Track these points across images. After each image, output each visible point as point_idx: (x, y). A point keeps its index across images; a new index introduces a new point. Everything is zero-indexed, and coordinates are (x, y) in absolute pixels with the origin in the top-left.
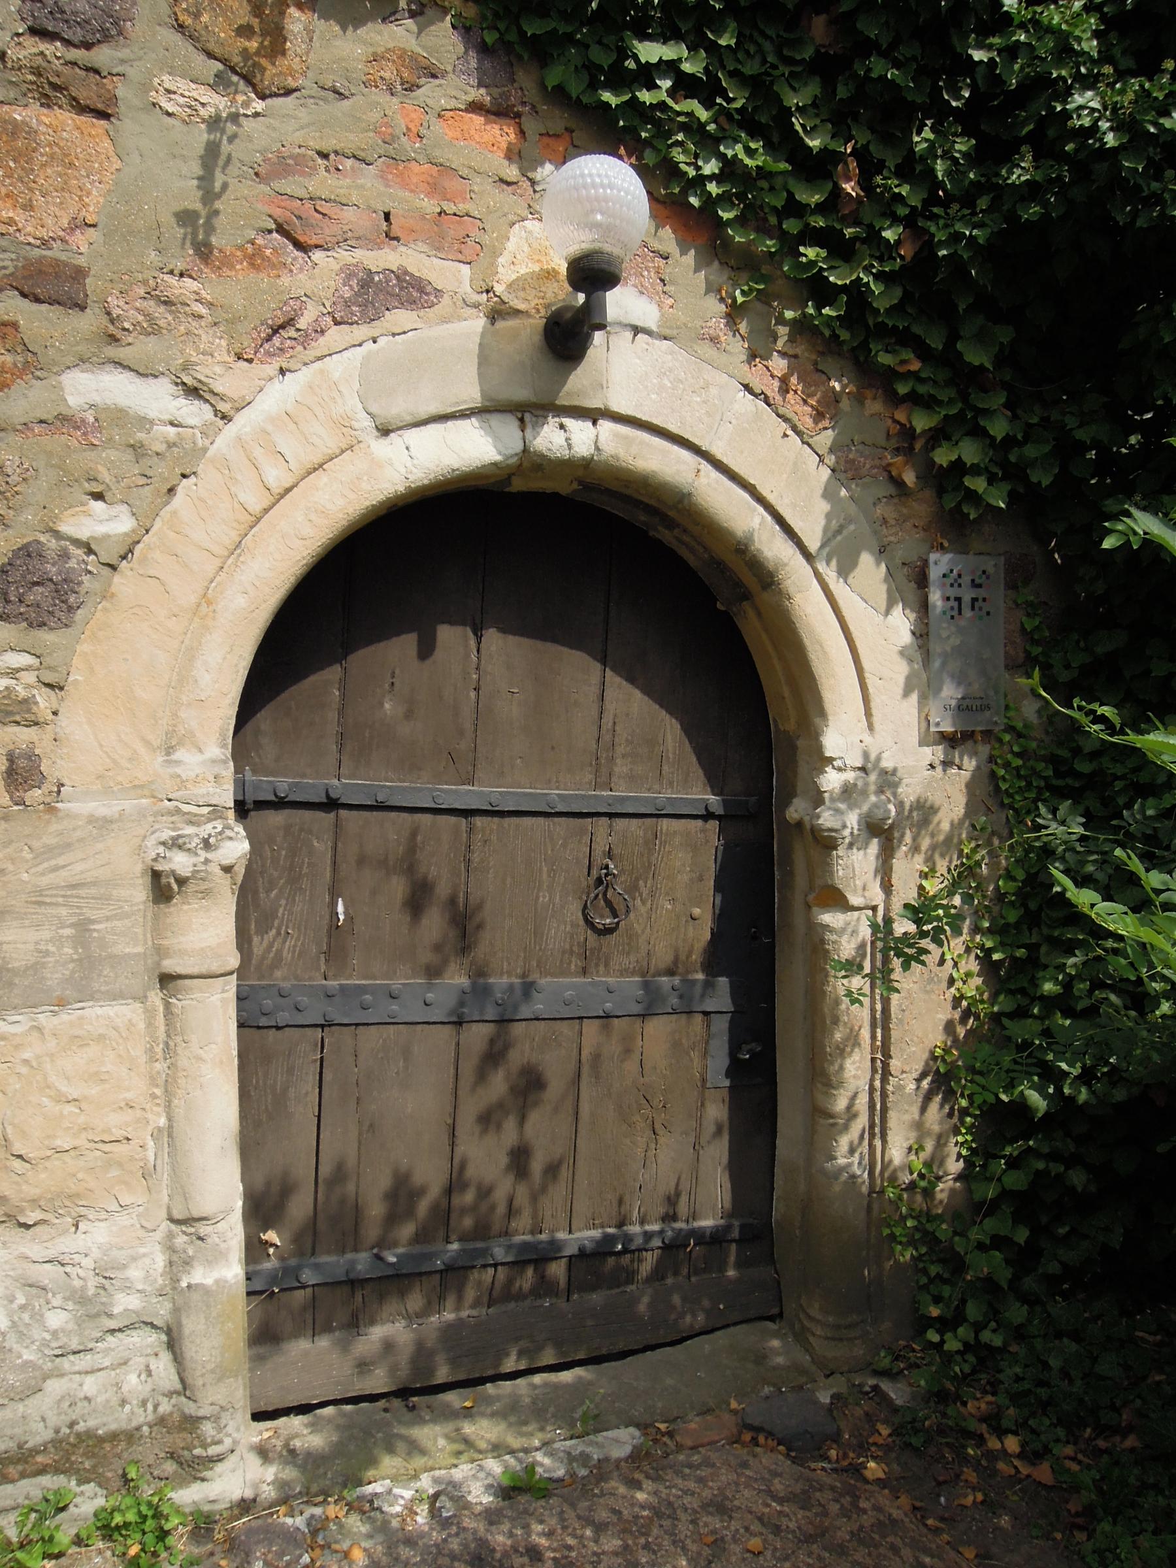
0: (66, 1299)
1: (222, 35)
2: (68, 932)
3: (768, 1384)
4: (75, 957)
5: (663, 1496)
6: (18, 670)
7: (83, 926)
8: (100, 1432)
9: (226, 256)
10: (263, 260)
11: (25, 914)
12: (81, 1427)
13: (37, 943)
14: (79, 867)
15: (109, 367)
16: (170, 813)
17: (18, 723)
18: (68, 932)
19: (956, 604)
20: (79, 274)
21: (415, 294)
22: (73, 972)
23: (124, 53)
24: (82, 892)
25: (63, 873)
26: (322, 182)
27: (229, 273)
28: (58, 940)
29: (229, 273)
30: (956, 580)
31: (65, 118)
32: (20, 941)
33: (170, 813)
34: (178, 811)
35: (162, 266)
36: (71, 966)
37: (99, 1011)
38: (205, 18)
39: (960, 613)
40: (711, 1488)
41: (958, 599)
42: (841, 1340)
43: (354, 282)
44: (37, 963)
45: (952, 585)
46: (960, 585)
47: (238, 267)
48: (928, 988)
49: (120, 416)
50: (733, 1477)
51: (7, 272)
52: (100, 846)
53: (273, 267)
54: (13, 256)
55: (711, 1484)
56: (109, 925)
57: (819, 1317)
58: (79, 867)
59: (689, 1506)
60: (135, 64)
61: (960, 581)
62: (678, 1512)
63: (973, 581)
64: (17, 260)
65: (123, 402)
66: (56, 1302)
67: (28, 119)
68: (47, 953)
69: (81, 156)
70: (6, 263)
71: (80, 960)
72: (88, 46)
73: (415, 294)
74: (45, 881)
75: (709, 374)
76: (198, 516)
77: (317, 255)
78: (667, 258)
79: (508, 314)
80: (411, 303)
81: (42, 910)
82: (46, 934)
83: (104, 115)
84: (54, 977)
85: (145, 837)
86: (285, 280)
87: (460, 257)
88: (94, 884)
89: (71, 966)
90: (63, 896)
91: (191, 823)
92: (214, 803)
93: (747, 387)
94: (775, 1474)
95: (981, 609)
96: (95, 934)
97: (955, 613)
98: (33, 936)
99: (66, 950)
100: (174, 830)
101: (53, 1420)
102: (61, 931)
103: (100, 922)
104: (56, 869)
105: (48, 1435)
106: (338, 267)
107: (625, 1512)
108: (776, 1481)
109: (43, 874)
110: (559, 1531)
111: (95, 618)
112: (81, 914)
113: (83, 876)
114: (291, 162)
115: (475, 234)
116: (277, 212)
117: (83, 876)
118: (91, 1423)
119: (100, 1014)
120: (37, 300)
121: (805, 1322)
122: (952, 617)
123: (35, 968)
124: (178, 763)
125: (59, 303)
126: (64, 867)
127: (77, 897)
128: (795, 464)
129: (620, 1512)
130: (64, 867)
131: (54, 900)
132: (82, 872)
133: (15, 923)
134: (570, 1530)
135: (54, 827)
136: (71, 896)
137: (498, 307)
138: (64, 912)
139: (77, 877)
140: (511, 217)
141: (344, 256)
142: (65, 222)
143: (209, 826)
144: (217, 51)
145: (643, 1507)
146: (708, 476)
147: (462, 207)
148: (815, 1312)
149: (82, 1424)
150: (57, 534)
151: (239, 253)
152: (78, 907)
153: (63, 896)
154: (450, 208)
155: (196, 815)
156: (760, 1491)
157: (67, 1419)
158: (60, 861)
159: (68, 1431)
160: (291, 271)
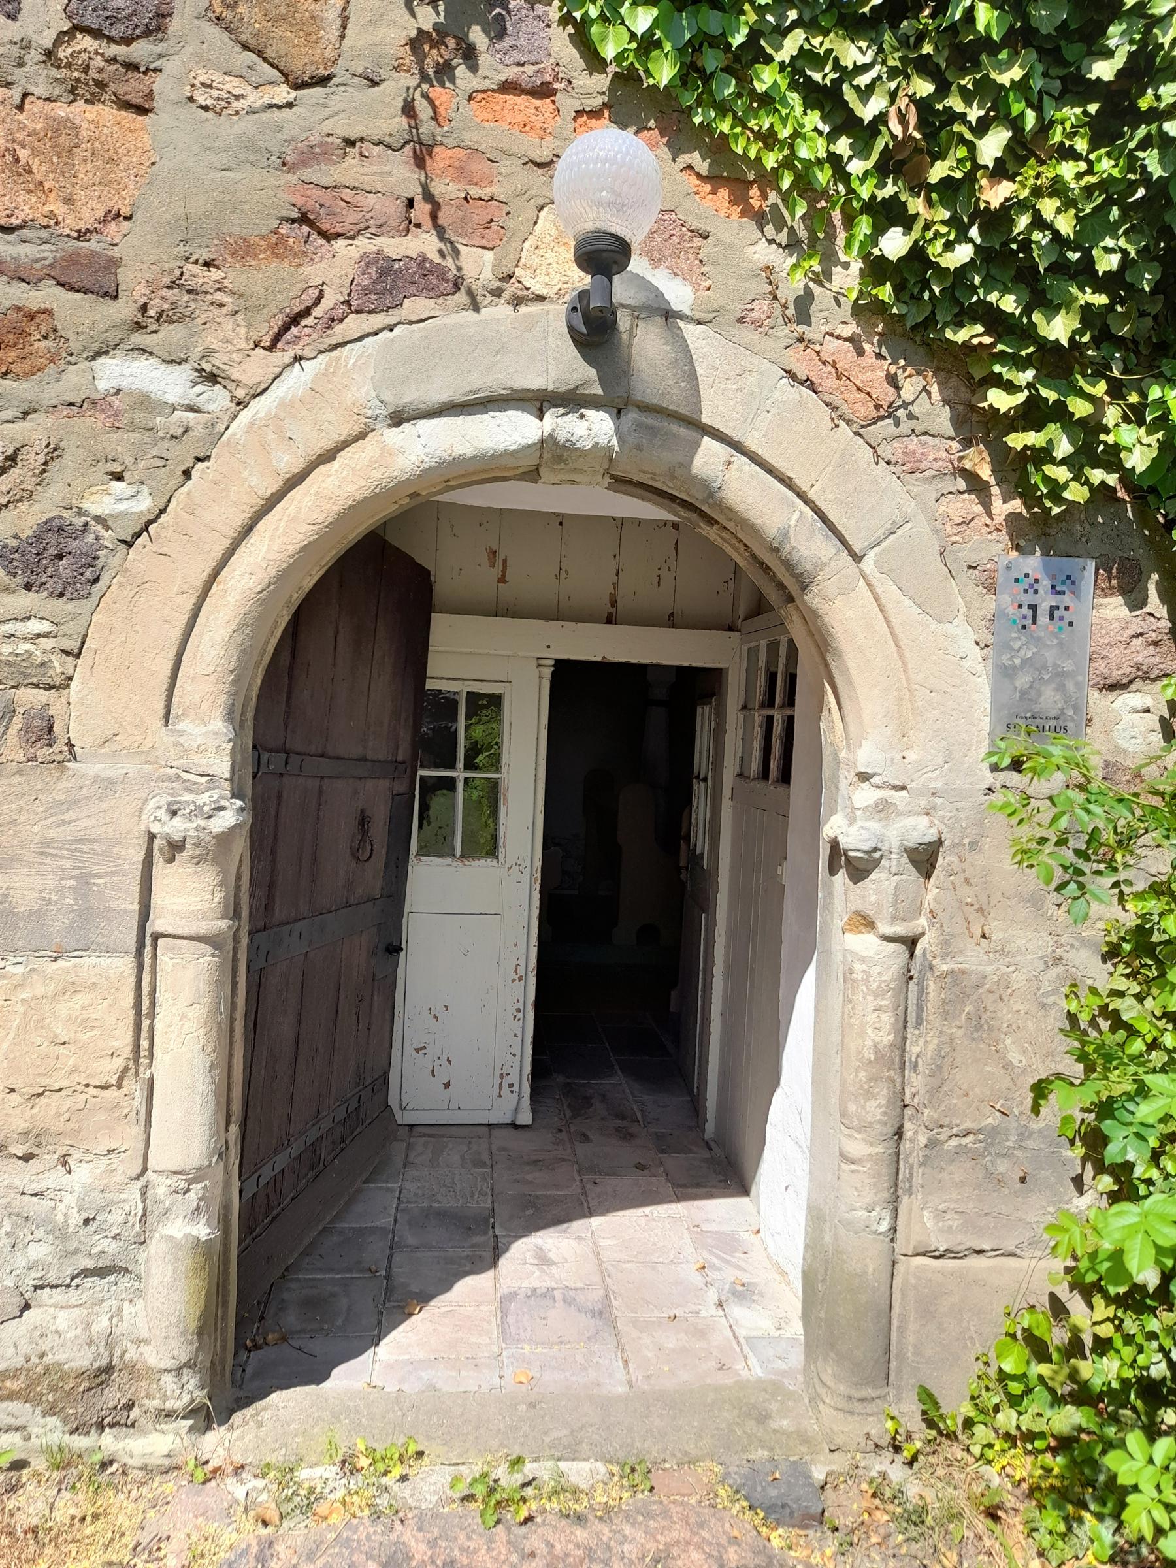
0: (47, 1233)
1: (257, 26)
2: (70, 883)
3: (763, 1447)
4: (76, 907)
5: (605, 1539)
6: (39, 636)
7: (84, 879)
8: (66, 1367)
9: (249, 246)
10: (286, 249)
11: (34, 863)
12: (48, 1359)
13: (41, 891)
14: (85, 823)
15: (135, 354)
16: (171, 780)
17: (37, 686)
18: (70, 883)
19: (1029, 613)
20: (113, 264)
21: (434, 281)
22: (73, 921)
23: (159, 48)
24: (86, 847)
25: (70, 828)
26: (350, 169)
27: (253, 262)
28: (59, 889)
29: (253, 262)
30: (1031, 586)
31: (106, 113)
32: (25, 888)
33: (171, 780)
34: (178, 777)
35: (187, 254)
36: (71, 915)
37: (93, 960)
38: (241, 9)
39: (1034, 622)
40: (658, 1542)
41: (1034, 608)
42: (852, 1413)
43: (373, 270)
44: (39, 910)
45: (1026, 591)
46: (1036, 592)
47: (262, 256)
48: (976, 1035)
49: (144, 402)
50: (685, 1534)
51: (47, 262)
52: (104, 806)
53: (295, 256)
54: (53, 248)
55: (659, 1537)
56: (108, 880)
57: (830, 1383)
58: (85, 823)
59: (627, 1555)
60: (171, 58)
61: (1036, 586)
62: (614, 1559)
63: (1053, 587)
64: (56, 251)
65: (147, 387)
66: (39, 1234)
67: (71, 116)
68: (49, 902)
69: (120, 150)
70: (46, 254)
71: (79, 911)
72: (127, 41)
73: (434, 281)
74: (53, 833)
75: (747, 360)
76: (213, 501)
77: (341, 243)
78: (706, 237)
79: (531, 300)
80: (432, 291)
81: (47, 861)
82: (50, 884)
83: (142, 111)
84: (56, 924)
85: (146, 800)
86: (307, 270)
87: (484, 243)
88: (96, 840)
89: (71, 915)
90: (68, 850)
91: (187, 790)
92: (212, 773)
93: (791, 375)
94: (734, 1541)
95: (1061, 619)
96: (95, 888)
97: (1028, 622)
98: (38, 884)
99: (67, 900)
100: (173, 795)
101: (25, 1348)
102: (64, 882)
103: (100, 877)
104: (63, 823)
105: (19, 1362)
106: (358, 255)
107: (558, 1547)
108: (732, 1550)
109: (50, 828)
110: (483, 1552)
111: (116, 590)
112: (82, 868)
113: (88, 833)
114: (317, 150)
115: (501, 219)
116: (300, 201)
117: (88, 833)
118: (61, 1357)
119: (91, 965)
120: (71, 289)
121: (818, 1390)
122: (1024, 627)
123: (36, 915)
124: (182, 733)
125: (93, 293)
126: (70, 822)
127: (81, 851)
128: (843, 456)
129: (553, 1546)
130: (70, 822)
131: (59, 852)
132: (86, 829)
133: (23, 871)
134: (495, 1553)
135: (63, 784)
136: (75, 850)
137: (519, 293)
138: (68, 864)
139: (82, 833)
140: (541, 201)
141: (364, 244)
142: (100, 213)
143: (208, 794)
144: (253, 42)
145: (578, 1547)
146: (740, 469)
147: (486, 193)
148: (828, 1379)
149: (50, 1356)
150: (81, 512)
151: (262, 243)
152: (80, 861)
153: (68, 850)
154: (474, 192)
155: (195, 783)
156: (710, 1556)
157: (38, 1351)
158: (67, 817)
159: (37, 1361)
160: (312, 260)
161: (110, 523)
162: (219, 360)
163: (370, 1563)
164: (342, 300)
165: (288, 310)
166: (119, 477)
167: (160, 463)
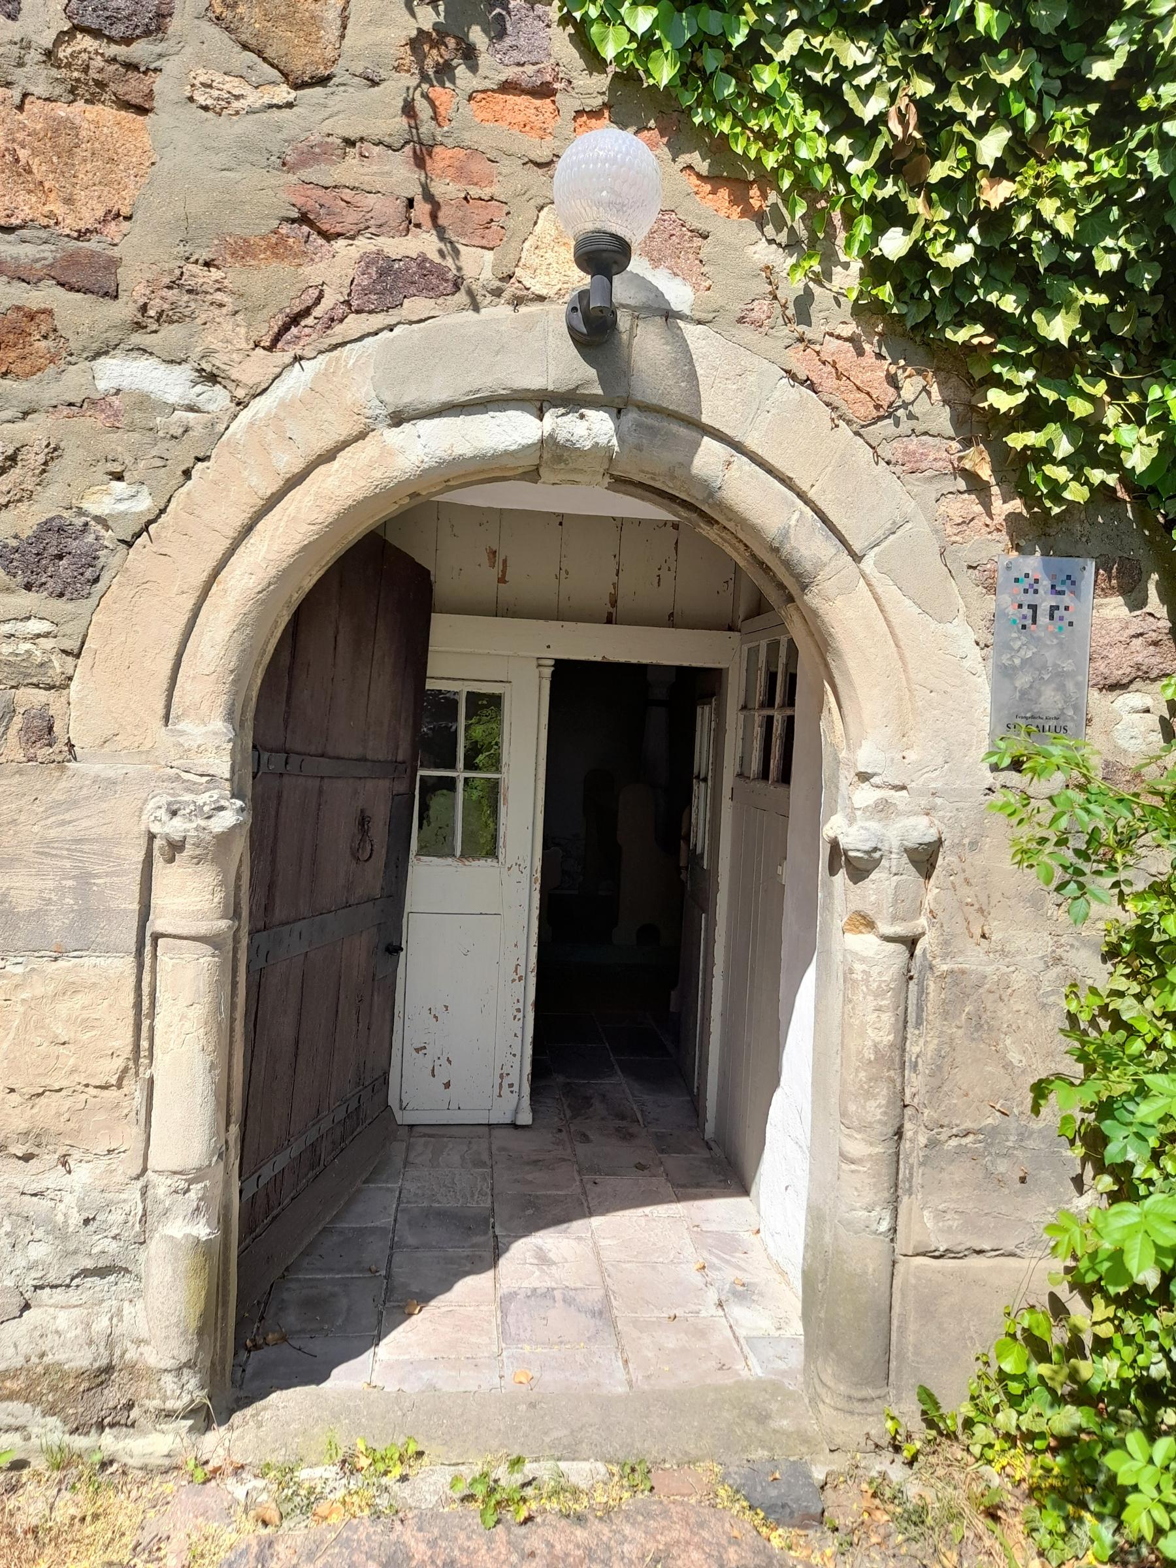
0: (47, 1233)
1: (257, 26)
2: (70, 883)
3: (763, 1447)
4: (76, 907)
5: (605, 1539)
6: (39, 636)
7: (84, 879)
8: (66, 1367)
9: (249, 246)
10: (286, 249)
11: (34, 863)
12: (48, 1359)
13: (41, 891)
14: (85, 823)
15: (135, 354)
16: (171, 780)
17: (37, 686)
18: (70, 883)
19: (1029, 613)
20: (113, 264)
21: (434, 281)
22: (73, 921)
23: (159, 48)
24: (86, 847)
25: (70, 828)
26: (350, 169)
27: (253, 262)
28: (59, 889)
29: (253, 262)
30: (1031, 586)
31: (106, 113)
32: (25, 888)
33: (171, 780)
34: (178, 777)
35: (187, 254)
36: (71, 915)
37: (93, 960)
38: (241, 9)
39: (1034, 622)
40: (658, 1542)
41: (1034, 608)
42: (852, 1413)
43: (373, 270)
44: (39, 910)
45: (1026, 591)
46: (1036, 592)
47: (262, 256)
48: (976, 1035)
49: (144, 402)
50: (685, 1534)
51: (47, 262)
52: (104, 806)
53: (295, 256)
54: (53, 248)
55: (659, 1537)
56: (108, 880)
57: (830, 1383)
58: (85, 823)
59: (627, 1555)
60: (171, 58)
61: (1036, 586)
62: (614, 1559)
63: (1053, 587)
64: (56, 251)
65: (147, 387)
66: (39, 1234)
67: (71, 116)
68: (49, 902)
69: (120, 150)
70: (46, 254)
71: (79, 911)
72: (127, 41)
73: (434, 281)
74: (53, 833)
75: (747, 360)
76: (213, 501)
77: (341, 243)
78: (706, 237)
79: (531, 300)
80: (432, 291)
81: (47, 861)
82: (50, 884)
83: (142, 111)
84: (56, 924)
85: (146, 800)
86: (307, 270)
87: (484, 243)
88: (96, 840)
89: (71, 915)
90: (68, 850)
91: (187, 790)
92: (212, 773)
93: (791, 375)
94: (734, 1541)
95: (1061, 619)
96: (95, 888)
97: (1028, 622)
98: (38, 884)
99: (67, 900)
100: (173, 795)
101: (25, 1348)
102: (64, 882)
103: (100, 877)
104: (63, 823)
105: (19, 1362)
106: (358, 255)
107: (558, 1547)
108: (732, 1550)
109: (50, 828)
110: (483, 1552)
111: (116, 590)
112: (82, 868)
113: (88, 833)
114: (317, 150)
115: (501, 219)
116: (300, 201)
117: (88, 833)
118: (61, 1357)
119: (91, 965)
120: (71, 289)
121: (818, 1390)
122: (1024, 627)
123: (36, 915)
124: (182, 733)
125: (93, 293)
126: (70, 822)
127: (81, 851)
128: (843, 456)
129: (553, 1546)
130: (70, 822)
131: (59, 852)
132: (86, 829)
133: (23, 871)
134: (495, 1553)
135: (63, 784)
136: (75, 850)
137: (519, 293)
138: (68, 864)
139: (82, 833)
140: (541, 201)
141: (364, 244)
142: (100, 213)
143: (208, 794)
144: (253, 42)
145: (578, 1547)
146: (740, 469)
147: (486, 193)
148: (828, 1379)
149: (50, 1356)
150: (81, 512)
151: (262, 243)
152: (80, 861)
153: (68, 850)
154: (474, 192)
155: (195, 783)
156: (710, 1556)
157: (38, 1351)
158: (67, 817)
159: (37, 1361)
160: (312, 260)
161: (110, 523)
162: (219, 360)
163: (370, 1563)
164: (342, 300)
165: (288, 310)
167: (160, 463)
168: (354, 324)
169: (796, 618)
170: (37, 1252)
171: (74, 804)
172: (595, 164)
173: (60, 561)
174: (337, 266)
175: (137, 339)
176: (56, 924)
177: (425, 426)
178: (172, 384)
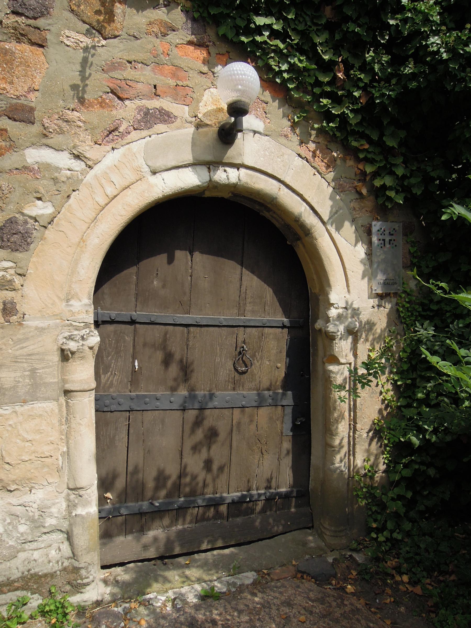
0: (26, 520)
2: (27, 373)
3: (308, 554)
4: (30, 383)
5: (266, 599)
6: (7, 268)
7: (33, 371)
8: (40, 573)
9: (90, 103)
10: (105, 104)
11: (10, 366)
12: (32, 572)
13: (15, 378)
14: (31, 347)
15: (44, 147)
16: (68, 326)
17: (7, 290)
18: (27, 373)
19: (383, 242)
20: (32, 110)
21: (166, 118)
22: (29, 389)
23: (50, 21)
24: (33, 357)
25: (25, 350)
26: (129, 73)
27: (92, 109)
28: (23, 377)
29: (92, 109)
30: (383, 232)
31: (26, 47)
32: (8, 377)
33: (68, 326)
34: (71, 325)
35: (65, 106)
36: (28, 387)
37: (40, 405)
39: (384, 246)
40: (285, 596)
41: (384, 240)
42: (337, 537)
43: (142, 113)
44: (15, 386)
45: (381, 234)
46: (384, 234)
47: (95, 107)
48: (372, 396)
49: (48, 167)
50: (293, 591)
51: (3, 109)
52: (40, 339)
53: (110, 107)
54: (5, 103)
55: (285, 594)
56: (43, 370)
57: (328, 527)
58: (31, 347)
59: (276, 603)
61: (384, 233)
62: (272, 605)
63: (390, 233)
64: (7, 104)
65: (49, 161)
66: (23, 521)
67: (11, 48)
68: (19, 382)
69: (32, 62)
70: (3, 105)
71: (32, 385)
73: (166, 118)
74: (18, 353)
75: (284, 150)
76: (79, 207)
77: (127, 102)
78: (267, 103)
79: (204, 126)
80: (165, 121)
81: (17, 364)
82: (18, 374)
83: (41, 46)
84: (22, 391)
85: (58, 335)
86: (114, 112)
87: (184, 103)
88: (38, 354)
89: (28, 387)
90: (25, 359)
91: (77, 330)
92: (86, 321)
93: (299, 155)
94: (311, 590)
95: (393, 244)
96: (38, 374)
97: (383, 245)
98: (13, 375)
99: (26, 380)
100: (70, 332)
101: (21, 569)
102: (24, 373)
103: (40, 369)
104: (22, 348)
105: (19, 575)
106: (135, 107)
107: (250, 606)
108: (311, 593)
109: (17, 350)
110: (224, 613)
111: (38, 248)
112: (32, 366)
113: (33, 351)
114: (116, 65)
115: (190, 94)
116: (111, 85)
117: (33, 351)
118: (37, 570)
119: (40, 406)
120: (15, 120)
121: (323, 530)
122: (381, 247)
123: (14, 388)
124: (71, 305)
125: (24, 122)
126: (26, 347)
127: (31, 359)
128: (318, 186)
129: (248, 606)
130: (26, 347)
131: (21, 360)
132: (33, 349)
133: (6, 370)
134: (228, 613)
135: (22, 331)
136: (29, 359)
137: (200, 123)
138: (25, 365)
139: (31, 351)
140: (205, 87)
141: (138, 102)
142: (26, 89)
143: (84, 331)
145: (257, 604)
146: (283, 191)
147: (185, 83)
148: (326, 525)
149: (33, 570)
150: (23, 214)
151: (96, 101)
152: (31, 363)
153: (25, 359)
154: (180, 83)
155: (78, 326)
156: (304, 597)
157: (27, 568)
158: (24, 345)
159: (27, 573)
160: (117, 108)
161: (37, 219)
162: (81, 149)
163: (183, 626)
164: (130, 125)
165: (108, 129)
166: (39, 199)
167: (57, 192)
168: (134, 134)
169: (301, 246)
170: (22, 528)
171: (27, 339)
172: (248, 77)
173: (10, 236)
174: (128, 111)
175: (45, 141)
176: (22, 391)
177: (165, 175)
178: (62, 160)
